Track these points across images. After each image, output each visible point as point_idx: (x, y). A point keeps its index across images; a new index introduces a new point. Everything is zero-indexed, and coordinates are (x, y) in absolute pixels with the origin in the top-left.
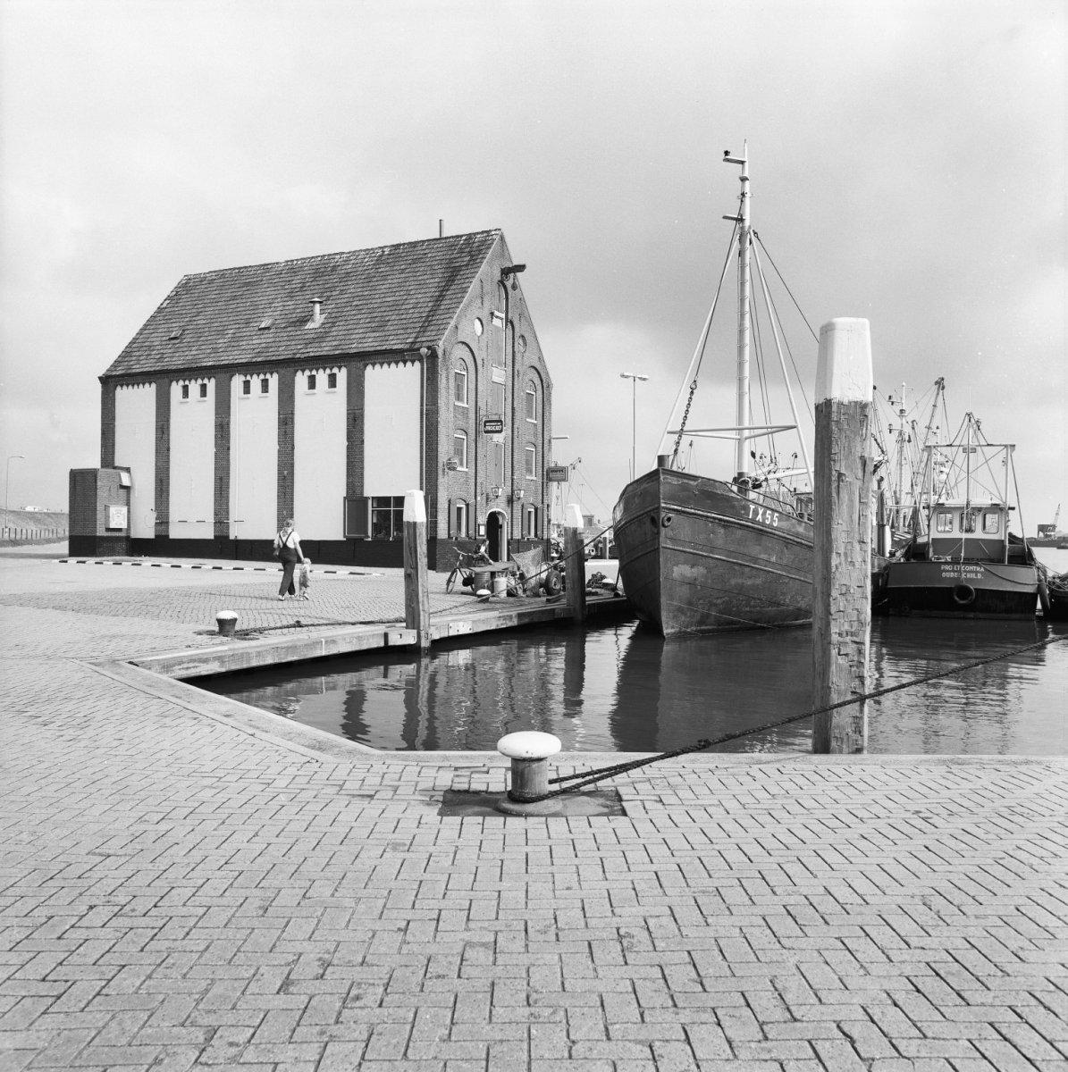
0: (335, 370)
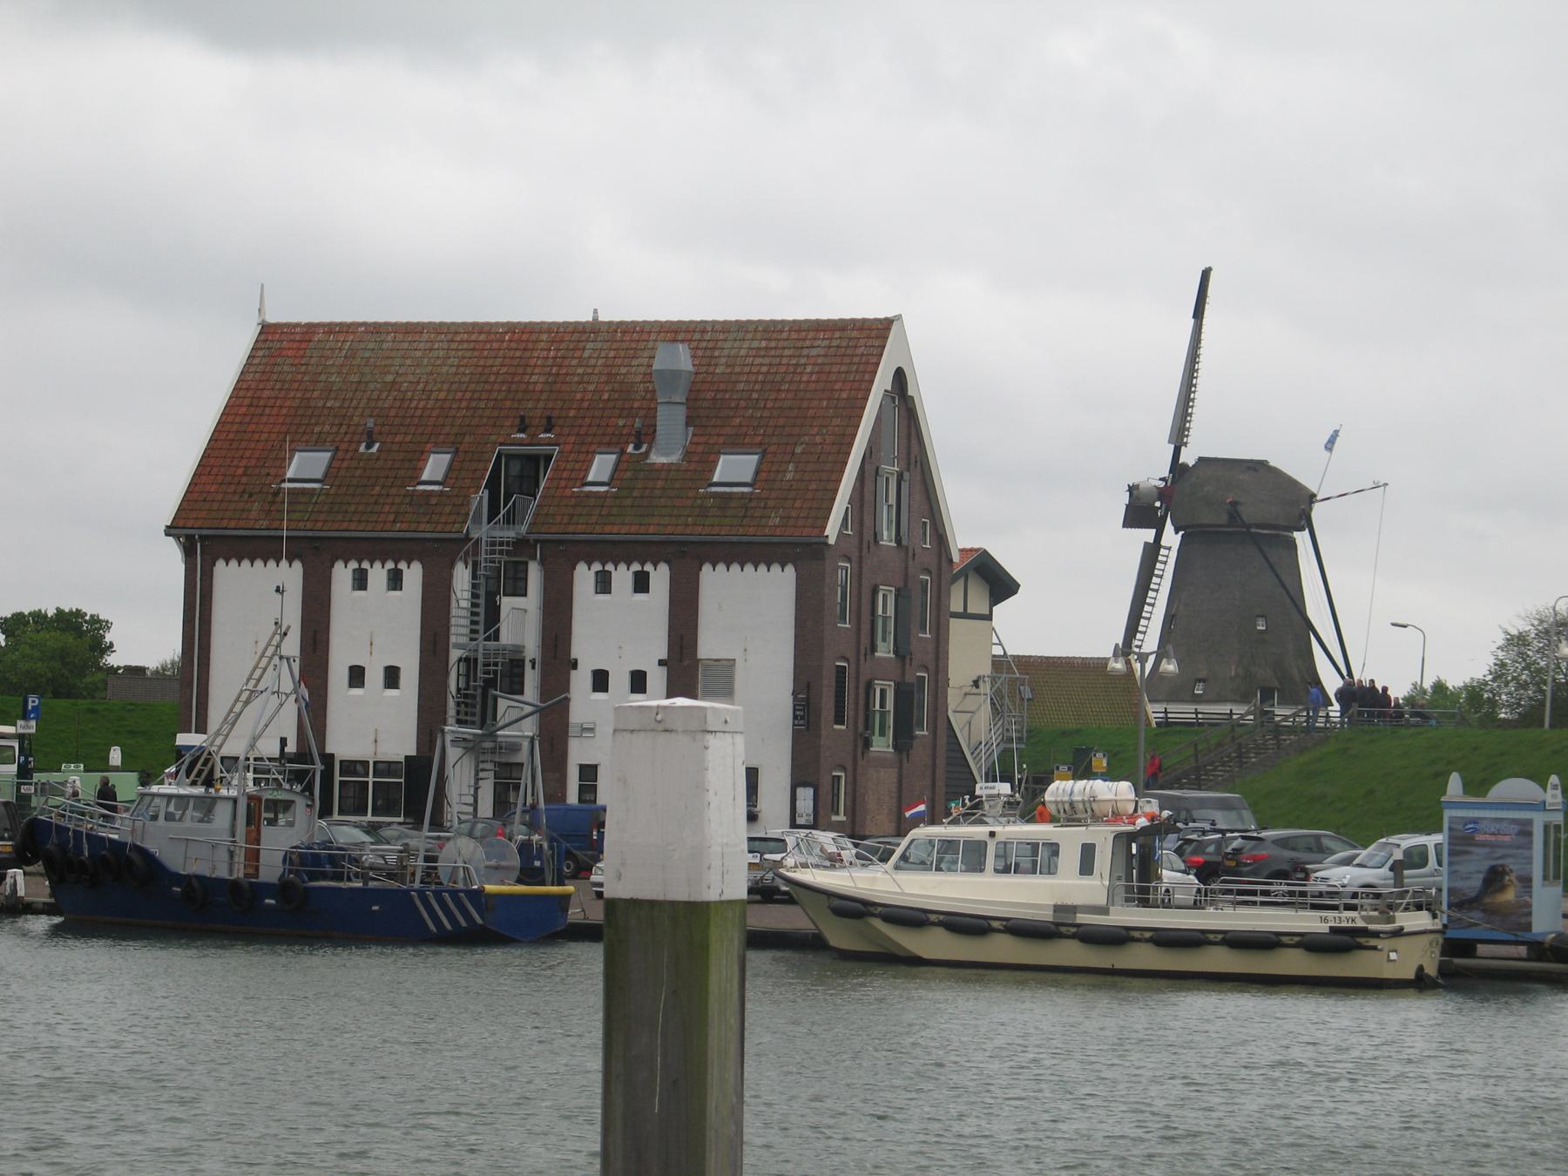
0: (402, 565)
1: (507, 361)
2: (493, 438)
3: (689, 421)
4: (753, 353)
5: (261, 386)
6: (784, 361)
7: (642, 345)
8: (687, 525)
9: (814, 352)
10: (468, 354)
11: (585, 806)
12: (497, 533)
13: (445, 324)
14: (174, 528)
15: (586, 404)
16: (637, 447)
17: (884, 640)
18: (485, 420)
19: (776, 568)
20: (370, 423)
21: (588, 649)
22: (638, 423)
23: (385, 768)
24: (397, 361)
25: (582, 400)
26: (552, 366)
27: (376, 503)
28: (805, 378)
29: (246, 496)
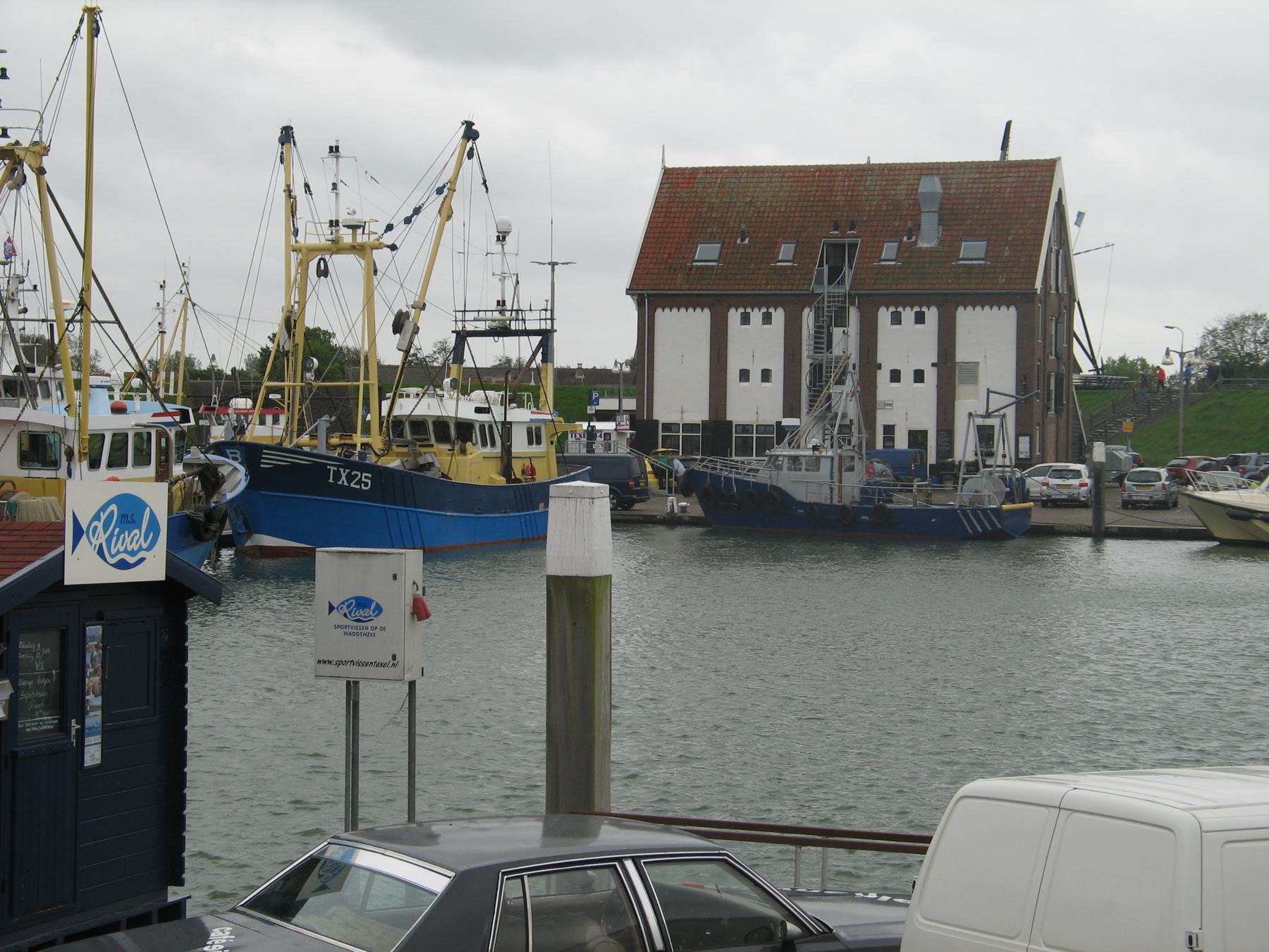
1: (819, 189)
2: (819, 234)
3: (940, 222)
4: (972, 181)
5: (670, 205)
6: (992, 185)
7: (901, 178)
8: (948, 284)
9: (1010, 180)
10: (795, 184)
11: (886, 450)
12: (833, 291)
13: (777, 167)
15: (873, 213)
16: (909, 238)
18: (811, 224)
20: (743, 226)
21: (887, 357)
22: (909, 224)
23: (688, 427)
24: (751, 190)
25: (870, 210)
26: (848, 191)
27: (753, 273)
28: (1006, 196)
29: (672, 271)
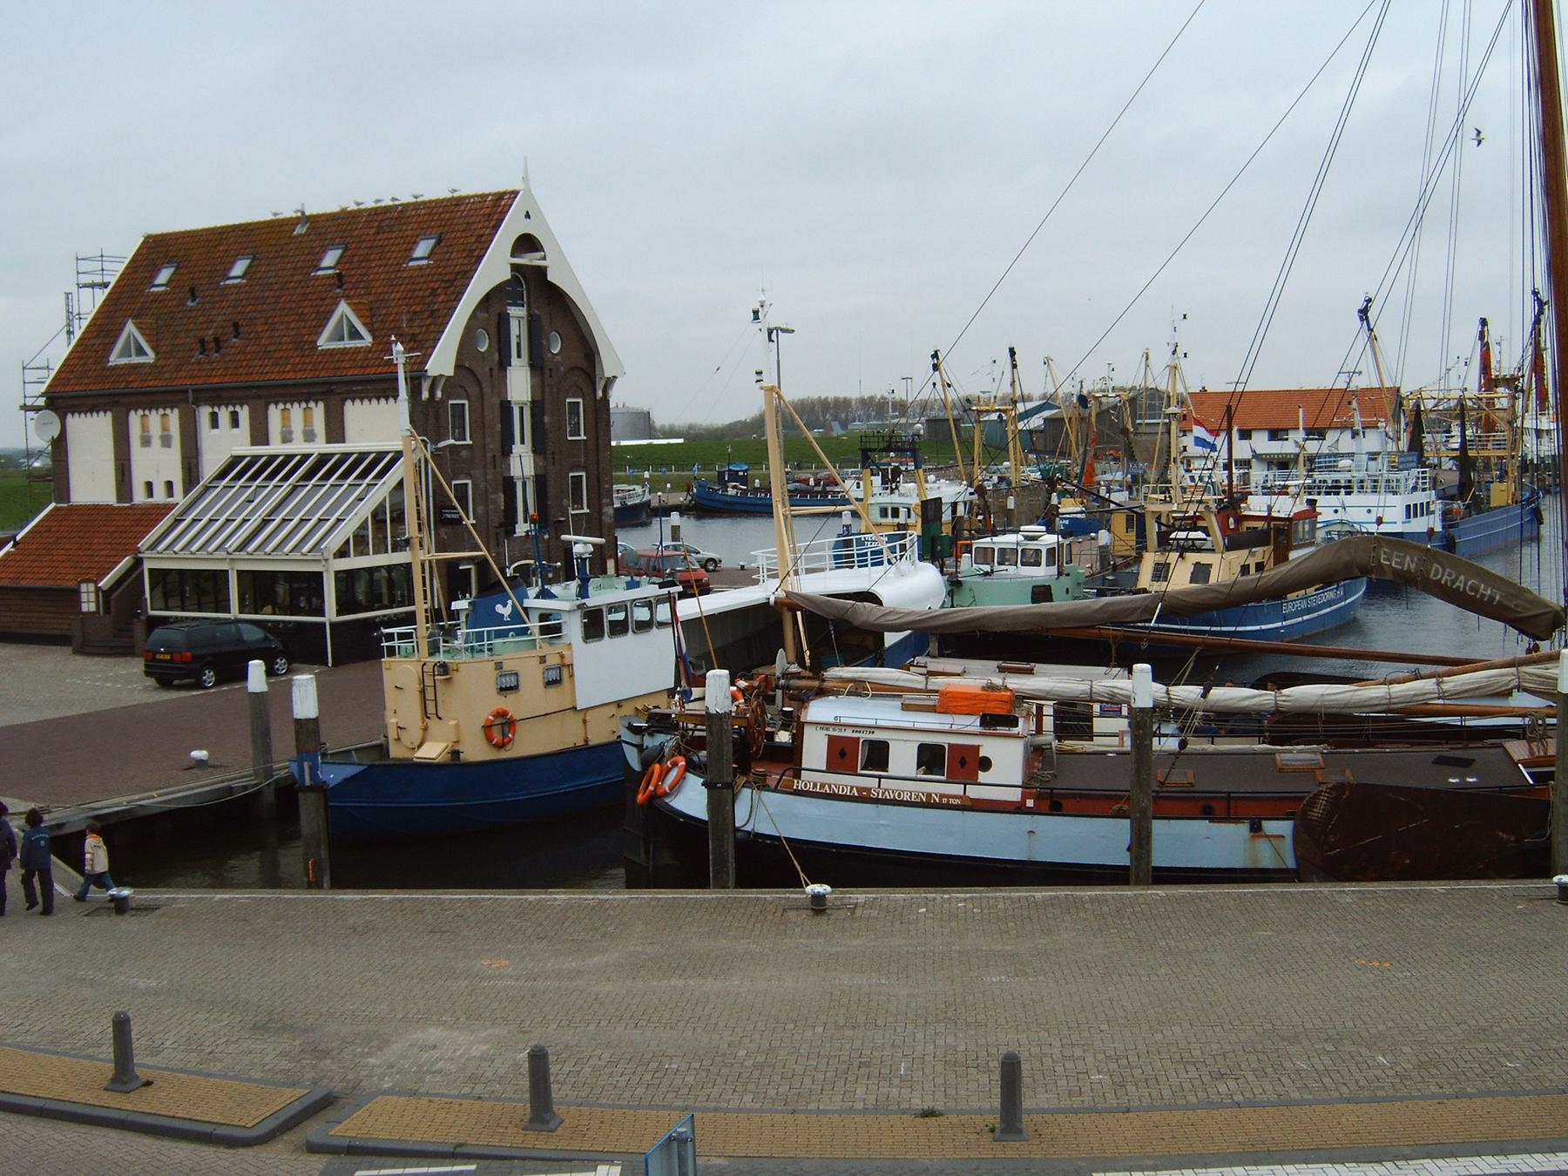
0: (238, 408)
14: (595, 1161)
17: (519, 356)
19: (102, 414)
